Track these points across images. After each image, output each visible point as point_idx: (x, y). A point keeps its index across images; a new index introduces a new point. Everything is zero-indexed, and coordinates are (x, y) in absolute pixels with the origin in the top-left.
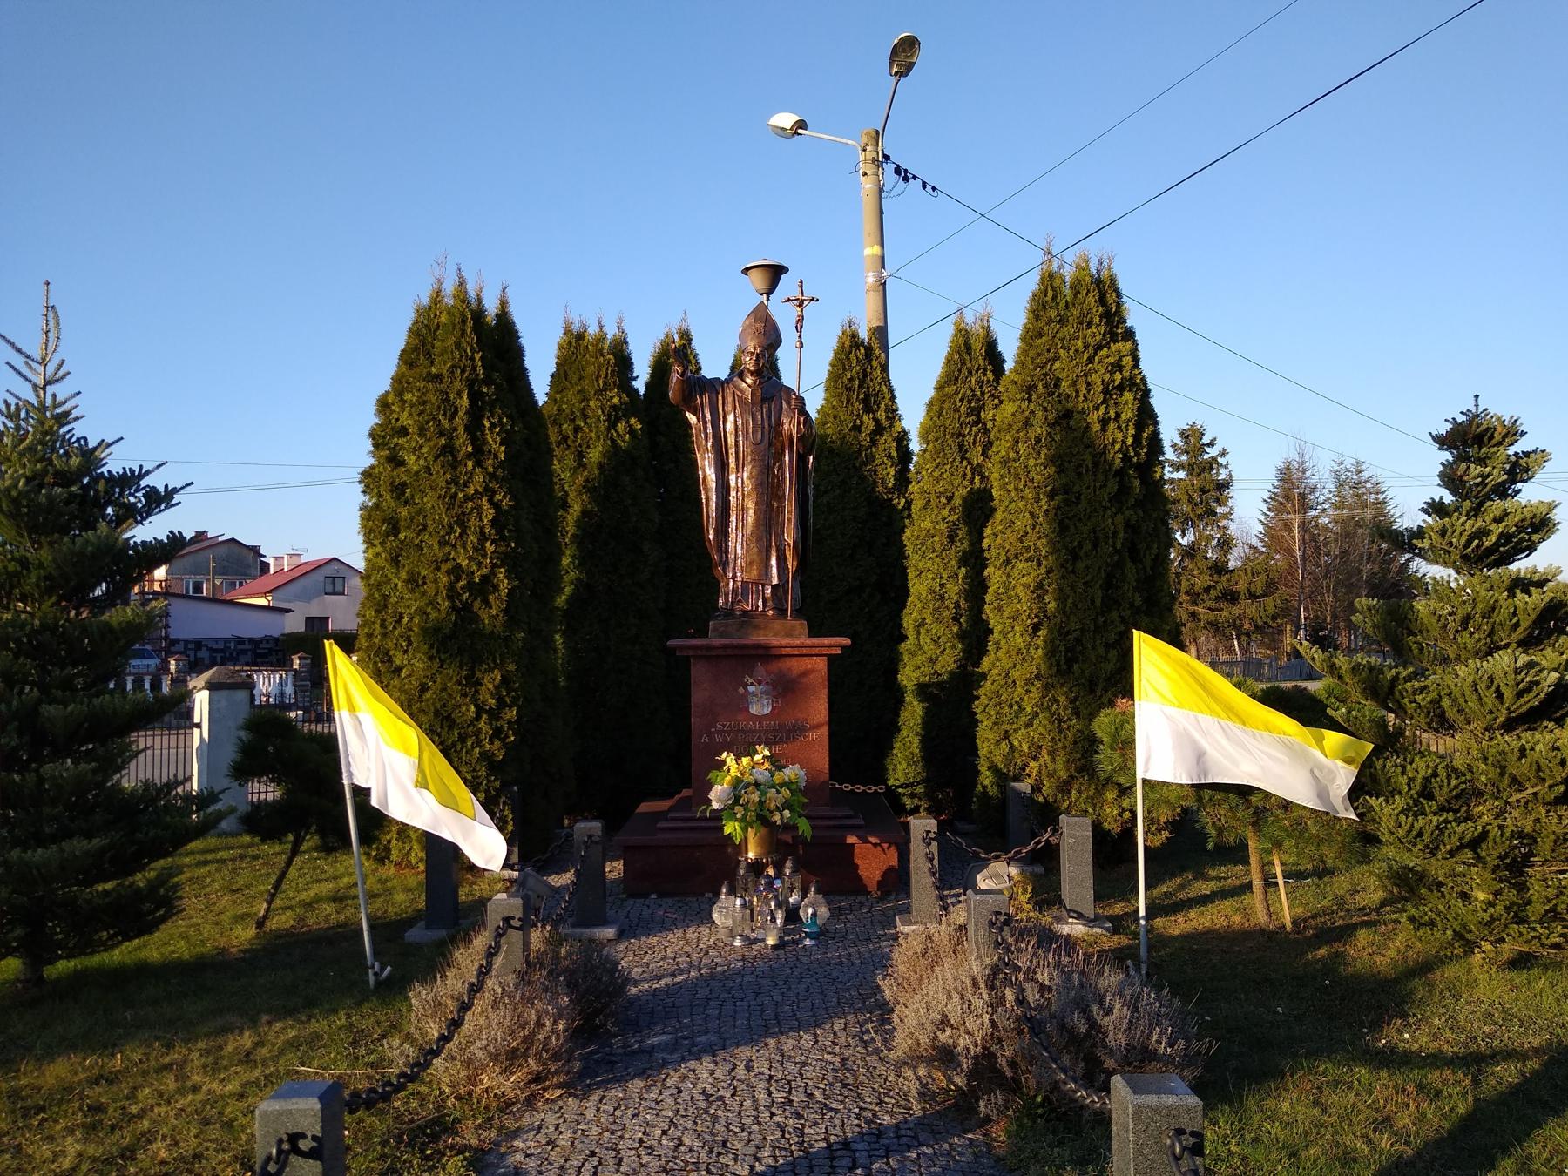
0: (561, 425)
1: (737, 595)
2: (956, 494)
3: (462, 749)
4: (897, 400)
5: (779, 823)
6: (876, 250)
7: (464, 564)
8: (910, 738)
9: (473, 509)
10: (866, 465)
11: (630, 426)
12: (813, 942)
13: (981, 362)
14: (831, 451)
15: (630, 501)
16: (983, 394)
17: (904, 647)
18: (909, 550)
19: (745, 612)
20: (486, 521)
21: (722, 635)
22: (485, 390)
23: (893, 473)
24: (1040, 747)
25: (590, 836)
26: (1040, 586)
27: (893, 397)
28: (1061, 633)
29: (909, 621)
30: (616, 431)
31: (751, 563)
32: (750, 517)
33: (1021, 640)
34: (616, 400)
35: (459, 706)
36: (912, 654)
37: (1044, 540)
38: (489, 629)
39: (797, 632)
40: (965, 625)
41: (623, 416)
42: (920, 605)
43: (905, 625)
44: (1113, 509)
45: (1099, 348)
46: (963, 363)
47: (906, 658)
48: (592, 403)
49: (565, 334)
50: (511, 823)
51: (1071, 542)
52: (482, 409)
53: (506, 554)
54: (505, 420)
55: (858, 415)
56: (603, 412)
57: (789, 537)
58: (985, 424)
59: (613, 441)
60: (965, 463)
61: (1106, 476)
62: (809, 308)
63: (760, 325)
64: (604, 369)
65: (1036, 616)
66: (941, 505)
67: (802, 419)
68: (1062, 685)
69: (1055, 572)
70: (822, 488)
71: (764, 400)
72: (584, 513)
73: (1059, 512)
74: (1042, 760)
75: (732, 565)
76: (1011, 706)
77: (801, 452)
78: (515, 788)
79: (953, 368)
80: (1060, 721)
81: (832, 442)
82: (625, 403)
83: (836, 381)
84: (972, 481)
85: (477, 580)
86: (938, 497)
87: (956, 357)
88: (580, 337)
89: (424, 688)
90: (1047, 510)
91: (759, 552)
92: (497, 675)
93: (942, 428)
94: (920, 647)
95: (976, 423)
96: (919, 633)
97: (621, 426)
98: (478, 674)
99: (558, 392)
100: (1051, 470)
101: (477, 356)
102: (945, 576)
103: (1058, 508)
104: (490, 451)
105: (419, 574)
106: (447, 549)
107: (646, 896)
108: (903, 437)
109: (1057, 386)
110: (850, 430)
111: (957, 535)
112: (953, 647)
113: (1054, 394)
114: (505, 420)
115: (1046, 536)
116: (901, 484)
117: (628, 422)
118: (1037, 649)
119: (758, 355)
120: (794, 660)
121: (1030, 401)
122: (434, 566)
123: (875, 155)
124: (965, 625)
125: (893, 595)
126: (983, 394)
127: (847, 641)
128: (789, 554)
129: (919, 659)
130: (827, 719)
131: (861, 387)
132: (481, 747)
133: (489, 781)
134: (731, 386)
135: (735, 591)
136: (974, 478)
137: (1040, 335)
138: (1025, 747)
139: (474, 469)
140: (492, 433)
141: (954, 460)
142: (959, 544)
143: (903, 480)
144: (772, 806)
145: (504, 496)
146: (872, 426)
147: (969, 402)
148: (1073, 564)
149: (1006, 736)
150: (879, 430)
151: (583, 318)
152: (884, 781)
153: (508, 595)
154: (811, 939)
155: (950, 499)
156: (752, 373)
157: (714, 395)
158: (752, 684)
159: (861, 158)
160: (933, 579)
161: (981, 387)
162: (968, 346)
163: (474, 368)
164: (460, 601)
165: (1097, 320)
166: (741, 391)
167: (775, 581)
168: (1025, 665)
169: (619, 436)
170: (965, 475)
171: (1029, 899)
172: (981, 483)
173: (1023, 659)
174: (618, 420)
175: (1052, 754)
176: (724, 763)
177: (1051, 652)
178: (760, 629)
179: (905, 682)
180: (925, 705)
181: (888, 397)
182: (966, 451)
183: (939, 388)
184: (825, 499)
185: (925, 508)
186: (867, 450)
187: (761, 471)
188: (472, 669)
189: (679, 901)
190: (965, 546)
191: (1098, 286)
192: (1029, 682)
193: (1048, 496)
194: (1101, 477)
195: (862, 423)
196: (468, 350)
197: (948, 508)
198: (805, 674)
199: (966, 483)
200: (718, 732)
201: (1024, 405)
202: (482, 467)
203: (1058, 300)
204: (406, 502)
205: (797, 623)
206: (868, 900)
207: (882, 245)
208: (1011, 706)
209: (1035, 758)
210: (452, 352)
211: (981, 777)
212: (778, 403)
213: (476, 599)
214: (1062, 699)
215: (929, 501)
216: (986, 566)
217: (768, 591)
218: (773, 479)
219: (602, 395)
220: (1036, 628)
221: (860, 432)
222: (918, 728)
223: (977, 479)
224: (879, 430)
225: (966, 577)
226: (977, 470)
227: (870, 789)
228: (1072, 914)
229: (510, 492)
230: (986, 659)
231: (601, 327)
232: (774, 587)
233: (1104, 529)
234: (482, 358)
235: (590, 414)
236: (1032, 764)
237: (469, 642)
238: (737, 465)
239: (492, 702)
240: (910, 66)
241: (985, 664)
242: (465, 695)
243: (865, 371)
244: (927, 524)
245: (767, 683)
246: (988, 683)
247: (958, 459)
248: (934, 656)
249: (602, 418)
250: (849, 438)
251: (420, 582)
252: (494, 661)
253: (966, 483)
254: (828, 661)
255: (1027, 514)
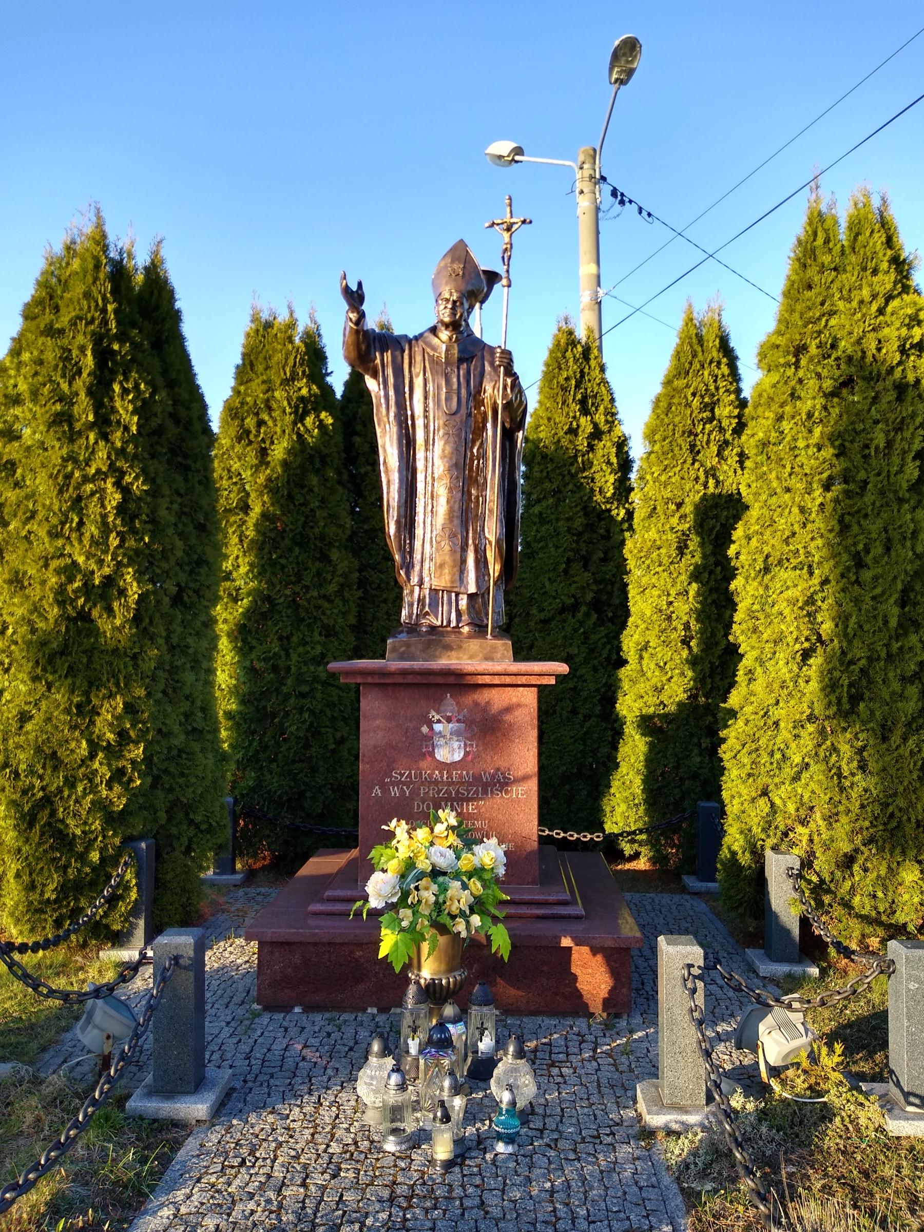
0: (243, 420)
1: (424, 606)
2: (687, 500)
3: (69, 796)
4: (616, 404)
5: (464, 934)
6: (593, 268)
7: (81, 560)
8: (630, 776)
9: (93, 494)
10: (584, 470)
11: (321, 421)
12: (511, 1149)
13: (715, 354)
14: (544, 457)
15: (317, 504)
16: (717, 389)
17: (623, 673)
18: (631, 564)
19: (433, 629)
20: (109, 508)
21: (402, 658)
22: (116, 347)
23: (612, 481)
24: (811, 808)
25: (176, 959)
26: (811, 601)
27: (612, 400)
28: (844, 660)
29: (630, 642)
30: (303, 425)
31: (442, 566)
32: (442, 507)
33: (785, 670)
34: (304, 392)
35: (67, 741)
36: (634, 682)
37: (819, 542)
38: (112, 644)
39: (499, 655)
40: (695, 650)
41: (313, 409)
42: (643, 626)
43: (625, 648)
44: (912, 502)
45: (889, 298)
46: (694, 355)
47: (626, 685)
48: (277, 394)
49: (252, 321)
50: (135, 889)
51: (855, 544)
52: (113, 372)
53: (137, 552)
54: (142, 386)
55: (574, 417)
56: (289, 404)
57: (492, 530)
58: (720, 422)
59: (300, 436)
60: (697, 465)
61: (903, 459)
62: (522, 235)
63: (458, 267)
64: (292, 358)
65: (807, 639)
66: (669, 512)
67: (509, 381)
68: (845, 730)
69: (833, 583)
70: (534, 497)
71: (461, 360)
72: (264, 515)
73: (839, 507)
74: (812, 825)
75: (417, 568)
76: (772, 754)
77: (507, 425)
78: (143, 845)
79: (683, 360)
80: (840, 775)
81: (545, 447)
82: (315, 395)
83: (551, 381)
84: (705, 486)
85: (97, 582)
86: (667, 503)
87: (687, 348)
88: (268, 325)
89: (24, 718)
90: (822, 504)
91: (452, 551)
92: (119, 702)
93: (671, 427)
94: (642, 673)
95: (711, 419)
96: (641, 658)
97: (309, 421)
98: (95, 701)
99: (241, 384)
100: (828, 452)
101: (110, 308)
102: (673, 592)
103: (836, 501)
104: (119, 422)
105: (25, 573)
106: (60, 542)
107: (286, 1008)
108: (622, 444)
109: (834, 346)
110: (566, 433)
111: (686, 547)
112: (682, 674)
113: (829, 356)
114: (142, 386)
115: (822, 536)
116: (620, 494)
117: (318, 416)
118: (807, 682)
119: (454, 302)
120: (494, 691)
121: (797, 365)
122: (41, 563)
123: (592, 172)
124: (695, 650)
125: (610, 614)
126: (717, 389)
127: (562, 668)
128: (490, 555)
129: (642, 687)
130: (536, 769)
131: (577, 386)
132: (95, 793)
133: (104, 837)
134: (420, 342)
135: (421, 601)
136: (707, 482)
137: (810, 287)
138: (791, 808)
139: (96, 443)
140: (123, 399)
141: (684, 462)
142: (689, 556)
143: (623, 489)
144: (454, 910)
145: (136, 478)
146: (590, 429)
147: (702, 397)
148: (856, 573)
149: (765, 793)
150: (597, 434)
151: (273, 306)
152: (600, 827)
153: (138, 603)
154: (507, 1143)
155: (679, 505)
156: (447, 326)
157: (398, 353)
158: (439, 721)
159: (578, 176)
160: (659, 596)
161: (715, 381)
162: (700, 339)
163: (105, 322)
164: (74, 608)
165: (884, 266)
166: (434, 349)
167: (472, 589)
168: (792, 702)
169: (307, 430)
170: (697, 479)
171: (838, 1064)
172: (716, 487)
173: (790, 694)
174: (306, 413)
175: (831, 819)
176: (391, 835)
177: (830, 686)
178: (452, 649)
179: (624, 712)
180: (648, 739)
181: (607, 399)
182: (698, 452)
183: (668, 383)
184: (537, 509)
185: (650, 516)
186: (583, 456)
187: (456, 449)
188: (87, 694)
189: (330, 1020)
190: (698, 559)
191: (883, 226)
192: (799, 725)
193: (823, 486)
194: (896, 460)
195: (578, 426)
196: (100, 302)
197: (677, 515)
198: (508, 709)
199: (698, 487)
200: (394, 784)
201: (790, 372)
202: (107, 440)
203: (831, 245)
204: (17, 485)
205: (499, 643)
206: (589, 1026)
207: (598, 263)
208: (772, 754)
209: (804, 822)
210: (79, 303)
211: (727, 840)
212: (479, 364)
213: (95, 605)
214: (845, 748)
215: (655, 509)
216: (733, 577)
217: (463, 603)
218: (472, 461)
219: (288, 385)
220: (806, 655)
221: (576, 435)
222: (641, 766)
223: (711, 482)
224: (597, 434)
225: (698, 594)
226: (711, 473)
227: (585, 837)
228: (912, 1099)
229: (144, 471)
230: (734, 692)
231: (291, 313)
232: (471, 597)
233: (900, 527)
234: (116, 311)
235: (275, 406)
236: (800, 829)
237: (85, 660)
238: (427, 442)
239: (110, 736)
240: (630, 73)
241: (734, 699)
242: (73, 728)
243: (582, 372)
244: (652, 534)
245: (459, 721)
246: (740, 723)
247: (690, 461)
248: (659, 685)
249: (288, 410)
250: (564, 442)
251: (26, 583)
252: (117, 685)
253: (698, 487)
254: (539, 692)
255: (795, 510)
